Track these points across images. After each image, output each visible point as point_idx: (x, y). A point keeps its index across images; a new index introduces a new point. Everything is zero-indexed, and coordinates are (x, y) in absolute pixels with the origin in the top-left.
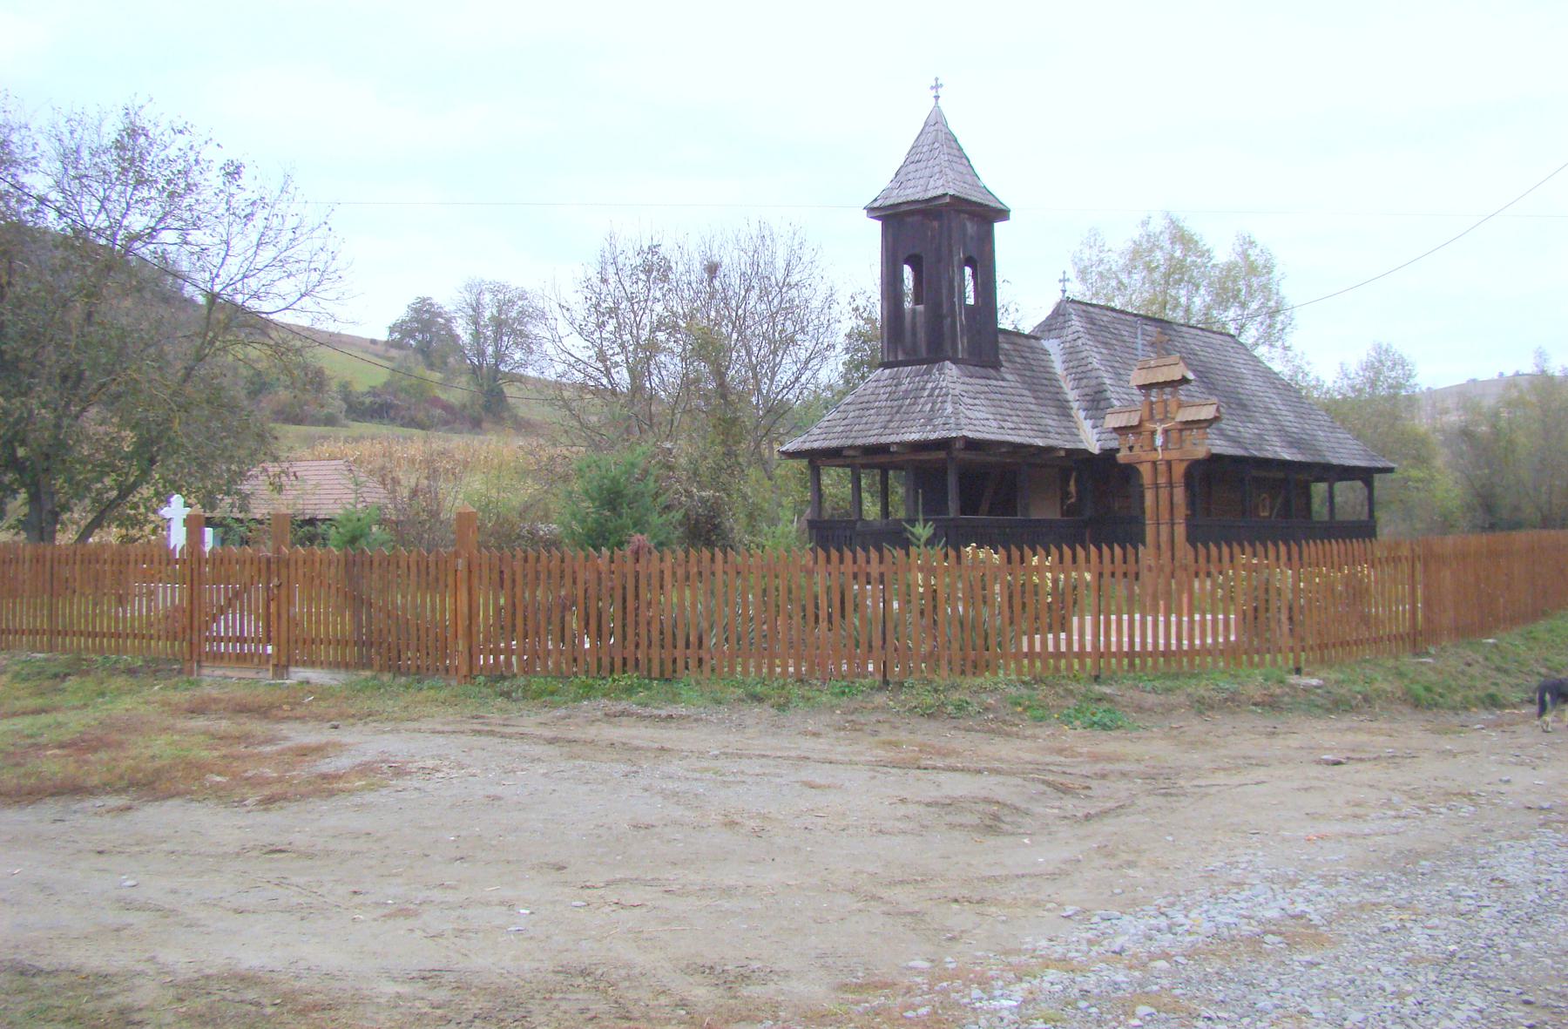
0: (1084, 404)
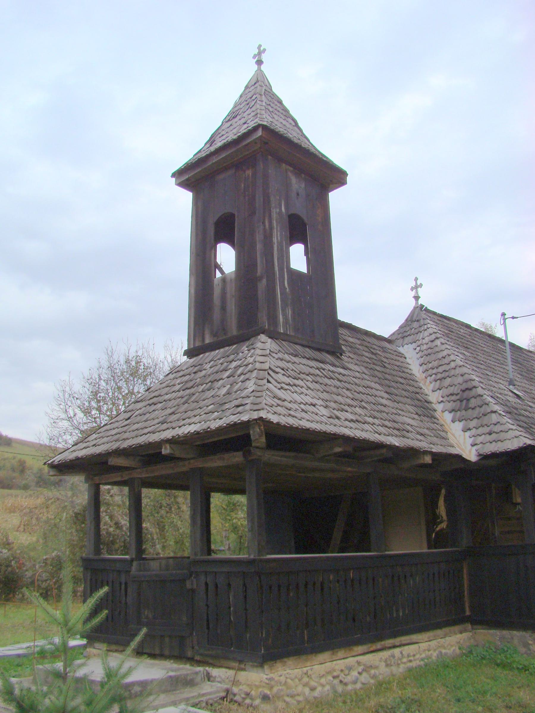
0: (450, 406)
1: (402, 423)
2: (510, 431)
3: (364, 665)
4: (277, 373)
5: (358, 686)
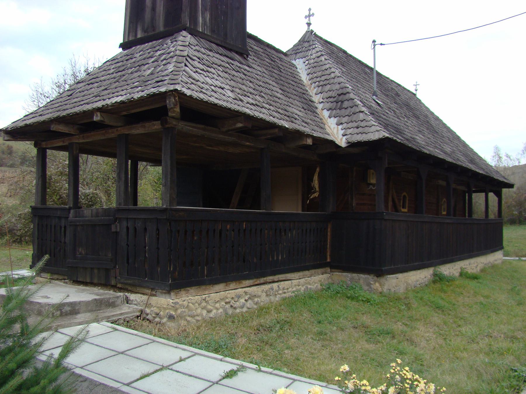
0: (328, 105)
1: (291, 113)
2: (373, 127)
3: (250, 294)
4: (194, 60)
5: (245, 310)
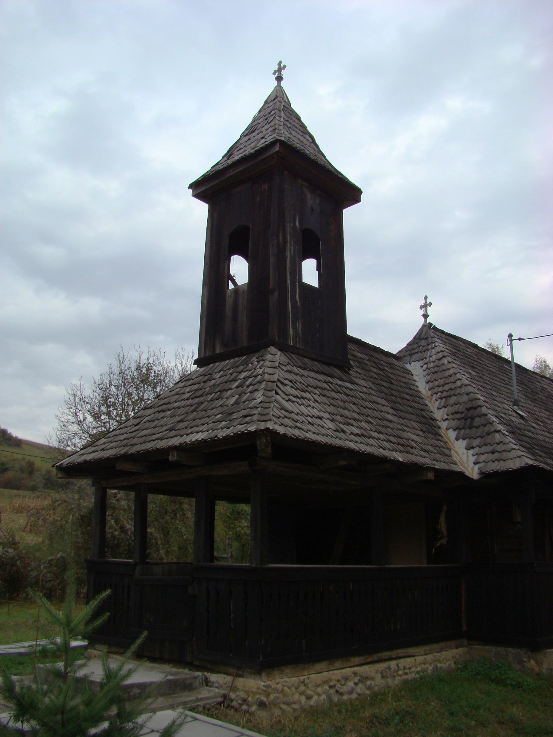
0: (454, 423)
1: (406, 439)
3: (360, 676)
4: (286, 385)
5: (354, 696)
